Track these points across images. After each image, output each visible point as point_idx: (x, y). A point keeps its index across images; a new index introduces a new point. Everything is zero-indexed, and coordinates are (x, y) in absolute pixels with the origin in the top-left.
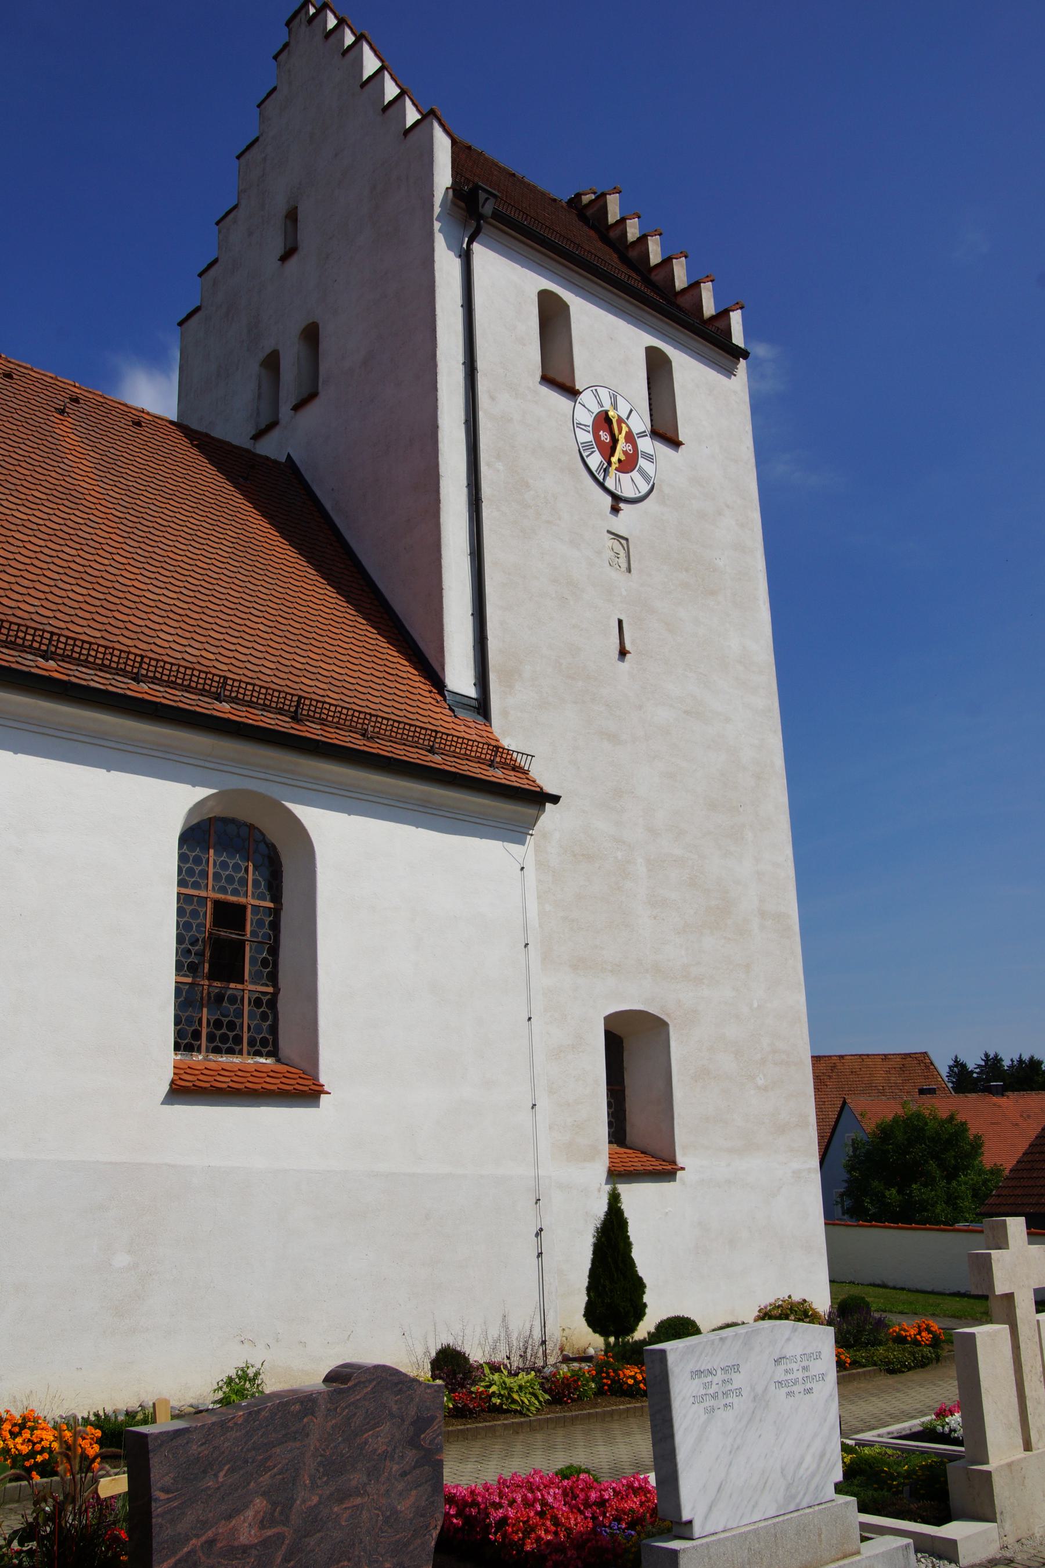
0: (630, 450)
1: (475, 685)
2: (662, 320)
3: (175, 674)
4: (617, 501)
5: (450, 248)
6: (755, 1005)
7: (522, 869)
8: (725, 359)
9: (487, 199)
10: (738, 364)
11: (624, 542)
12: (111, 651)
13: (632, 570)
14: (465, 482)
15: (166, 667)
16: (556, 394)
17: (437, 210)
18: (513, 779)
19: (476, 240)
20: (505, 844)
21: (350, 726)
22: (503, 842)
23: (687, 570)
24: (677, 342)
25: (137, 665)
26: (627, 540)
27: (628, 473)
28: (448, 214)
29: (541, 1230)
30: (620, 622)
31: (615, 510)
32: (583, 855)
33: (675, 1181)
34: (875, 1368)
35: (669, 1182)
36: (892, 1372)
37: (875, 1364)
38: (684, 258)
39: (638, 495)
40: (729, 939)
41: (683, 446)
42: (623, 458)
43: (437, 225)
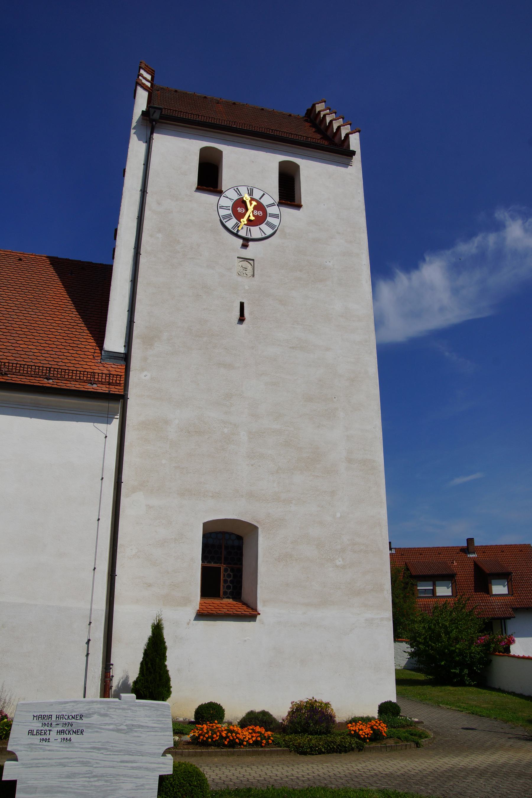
0: (261, 214)
1: (125, 346)
2: (292, 147)
3: (66, 374)
4: (246, 242)
5: (140, 139)
6: (338, 515)
7: (106, 437)
8: (343, 159)
9: (155, 112)
10: (352, 159)
11: (251, 262)
12: (30, 367)
13: (255, 275)
14: (133, 247)
15: (32, 368)
16: (206, 195)
17: (134, 124)
18: (69, 385)
19: (155, 131)
20: (95, 424)
21: (27, 373)
22: (94, 423)
23: (301, 271)
24: (298, 154)
25: (48, 372)
26: (253, 260)
27: (258, 226)
28: (141, 125)
29: (89, 640)
30: (242, 305)
31: (245, 246)
32: (196, 432)
33: (255, 621)
34: (287, 749)
35: (250, 621)
36: (304, 753)
37: (288, 747)
38: (341, 119)
39: (264, 236)
40: (317, 476)
41: (195, 190)
42: (252, 218)
43: (133, 131)
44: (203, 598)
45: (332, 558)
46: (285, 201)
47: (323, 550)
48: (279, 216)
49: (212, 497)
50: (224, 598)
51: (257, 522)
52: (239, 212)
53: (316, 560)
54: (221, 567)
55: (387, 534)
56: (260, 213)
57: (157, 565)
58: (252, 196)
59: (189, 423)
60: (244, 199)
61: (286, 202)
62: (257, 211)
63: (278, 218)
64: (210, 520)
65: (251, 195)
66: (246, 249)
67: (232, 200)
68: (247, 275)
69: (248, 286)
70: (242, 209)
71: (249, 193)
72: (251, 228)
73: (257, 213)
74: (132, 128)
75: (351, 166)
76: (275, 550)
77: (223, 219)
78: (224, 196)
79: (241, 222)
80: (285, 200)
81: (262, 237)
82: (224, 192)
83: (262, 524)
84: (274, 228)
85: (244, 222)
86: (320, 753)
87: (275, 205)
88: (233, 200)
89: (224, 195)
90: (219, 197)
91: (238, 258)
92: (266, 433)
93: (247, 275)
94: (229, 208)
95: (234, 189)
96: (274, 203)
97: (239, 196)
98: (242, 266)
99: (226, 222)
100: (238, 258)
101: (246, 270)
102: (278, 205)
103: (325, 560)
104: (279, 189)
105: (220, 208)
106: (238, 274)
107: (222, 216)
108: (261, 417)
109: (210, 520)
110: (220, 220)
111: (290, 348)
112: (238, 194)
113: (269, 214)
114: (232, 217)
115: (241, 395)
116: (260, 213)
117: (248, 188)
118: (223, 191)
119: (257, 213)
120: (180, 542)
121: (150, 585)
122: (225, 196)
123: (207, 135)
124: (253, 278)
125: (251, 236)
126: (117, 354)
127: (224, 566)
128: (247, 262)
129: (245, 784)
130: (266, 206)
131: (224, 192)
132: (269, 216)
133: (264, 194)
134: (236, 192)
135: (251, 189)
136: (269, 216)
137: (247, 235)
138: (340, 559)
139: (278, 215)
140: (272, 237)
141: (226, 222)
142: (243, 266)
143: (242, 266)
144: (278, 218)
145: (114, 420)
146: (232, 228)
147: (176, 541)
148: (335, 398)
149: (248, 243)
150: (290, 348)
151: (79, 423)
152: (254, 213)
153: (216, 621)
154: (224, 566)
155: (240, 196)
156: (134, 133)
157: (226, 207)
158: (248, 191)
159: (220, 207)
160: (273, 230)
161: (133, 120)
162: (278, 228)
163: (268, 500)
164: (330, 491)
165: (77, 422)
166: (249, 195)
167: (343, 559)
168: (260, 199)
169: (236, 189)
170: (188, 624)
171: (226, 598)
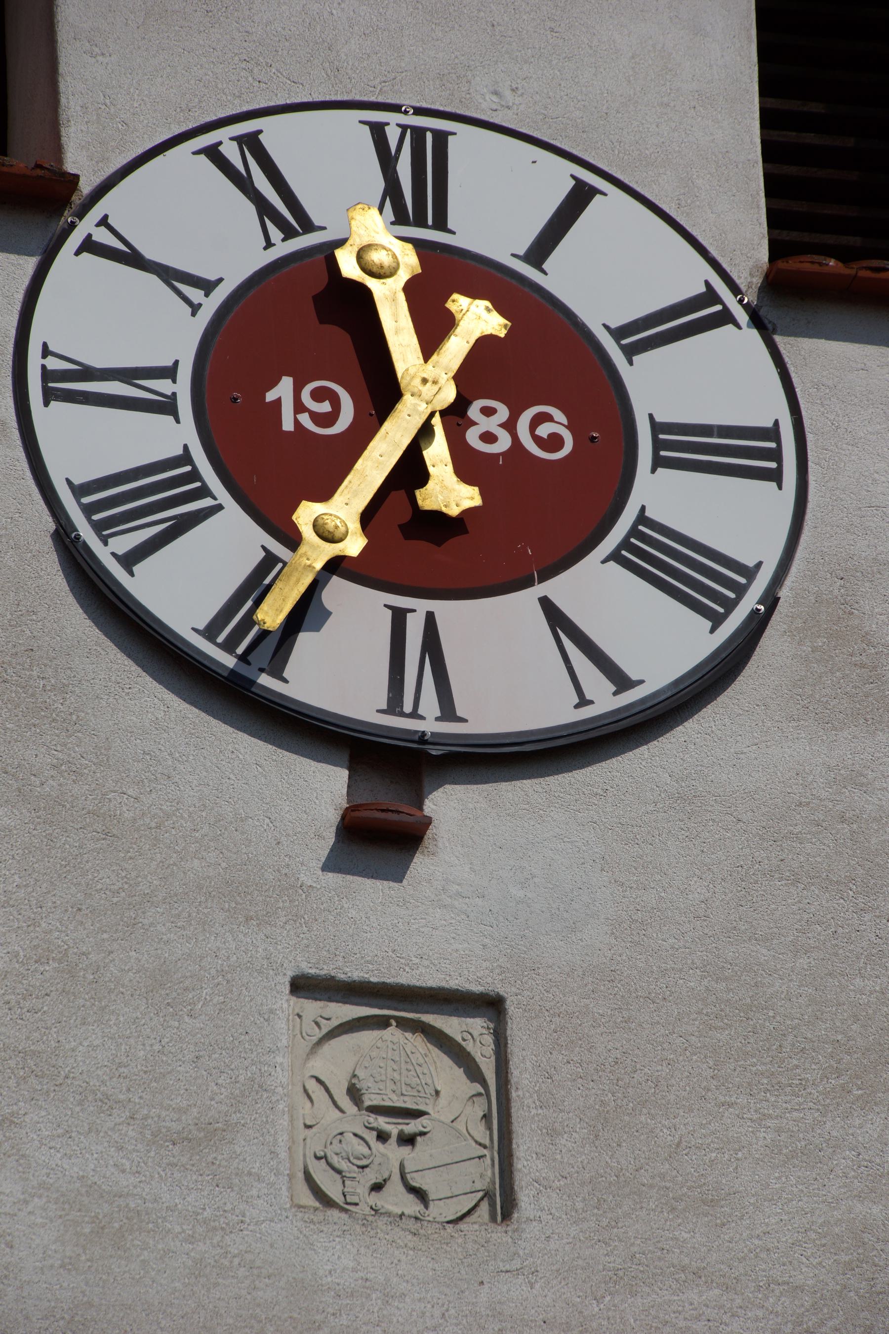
0: (554, 443)
13: (525, 1197)
27: (525, 583)
46: (845, 255)
48: (776, 455)
52: (288, 425)
55: (398, 445)
56: (544, 430)
58: (441, 224)
60: (349, 267)
61: (860, 270)
62: (503, 412)
63: (776, 476)
65: (420, 222)
66: (399, 878)
67: (195, 294)
68: (420, 1194)
70: (318, 395)
71: (392, 189)
72: (442, 608)
73: (510, 426)
77: (99, 527)
78: (89, 246)
79: (293, 540)
80: (855, 241)
81: (587, 713)
82: (86, 187)
84: (730, 606)
85: (328, 537)
87: (725, 318)
88: (208, 286)
89: (87, 226)
90: (30, 264)
93: (420, 1194)
94: (164, 386)
95: (213, 153)
96: (710, 296)
97: (276, 234)
98: (354, 1093)
101: (408, 1140)
102: (757, 320)
104: (768, 119)
105: (49, 396)
106: (309, 1199)
107: (79, 491)
112: (264, 208)
113: (657, 427)
114: (204, 492)
116: (544, 430)
117: (378, 131)
118: (73, 180)
119: (510, 426)
122: (103, 236)
124: (498, 1234)
125: (448, 711)
128: (416, 1043)
129: (495, 96)
130: (619, 333)
131: (86, 187)
132: (658, 463)
134: (244, 184)
135: (418, 133)
136: (658, 463)
137: (394, 705)
139: (773, 433)
140: (708, 712)
141: (129, 560)
142: (365, 1083)
143: (354, 1093)
144: (776, 476)
146: (210, 632)
149: (420, 806)
152: (472, 437)
155: (289, 233)
157: (128, 375)
158: (387, 161)
159: (47, 375)
160: (717, 621)
162: (771, 600)
166: (400, 218)
169: (231, 151)
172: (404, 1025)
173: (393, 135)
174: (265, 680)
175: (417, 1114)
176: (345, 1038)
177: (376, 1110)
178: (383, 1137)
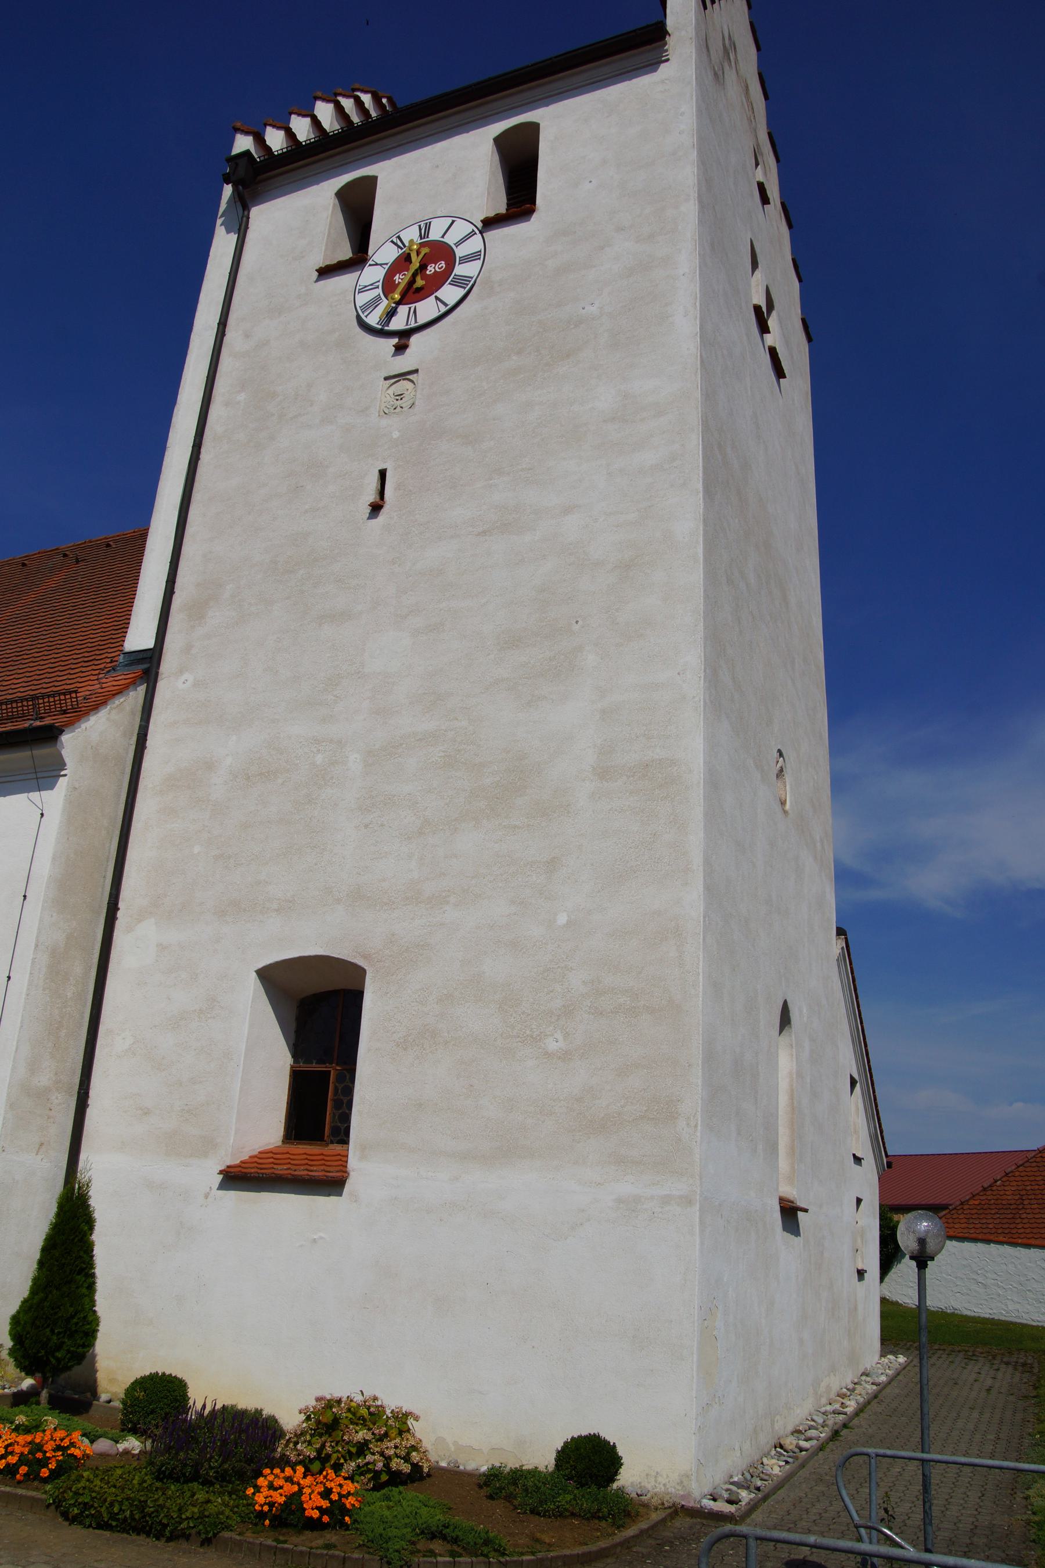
5: (228, 232)
6: (562, 919)
10: (666, 44)
33: (340, 1195)
35: (329, 1195)
39: (443, 309)
40: (515, 827)
43: (219, 221)
44: (288, 1143)
45: (538, 1033)
47: (514, 1015)
49: (277, 910)
50: (332, 1142)
51: (365, 957)
53: (495, 1040)
54: (330, 1071)
57: (164, 1070)
59: (251, 759)
64: (268, 962)
69: (399, 431)
74: (219, 216)
75: (667, 60)
76: (399, 1022)
81: (440, 313)
83: (376, 960)
86: (99, 1527)
91: (386, 379)
92: (404, 745)
97: (400, 250)
99: (416, 322)
100: (386, 379)
103: (518, 1040)
108: (397, 711)
109: (268, 963)
110: (358, 317)
111: (479, 534)
115: (359, 673)
117: (392, 242)
120: (209, 1015)
121: (147, 1112)
123: (349, 160)
126: (134, 654)
127: (338, 1068)
128: (405, 382)
133: (453, 222)
138: (559, 1035)
145: (61, 779)
147: (201, 1015)
148: (577, 622)
150: (479, 534)
151: (8, 798)
153: (260, 1192)
154: (338, 1068)
155: (402, 249)
156: (221, 225)
158: (396, 244)
160: (360, 307)
161: (222, 201)
162: (475, 282)
163: (394, 903)
164: (545, 859)
165: (5, 796)
167: (566, 1035)
168: (443, 237)
170: (206, 1196)
171: (337, 1143)
172: (404, 379)
173: (395, 240)
174: (386, 328)
175: (402, 395)
176: (394, 385)
177: (396, 396)
178: (397, 400)
